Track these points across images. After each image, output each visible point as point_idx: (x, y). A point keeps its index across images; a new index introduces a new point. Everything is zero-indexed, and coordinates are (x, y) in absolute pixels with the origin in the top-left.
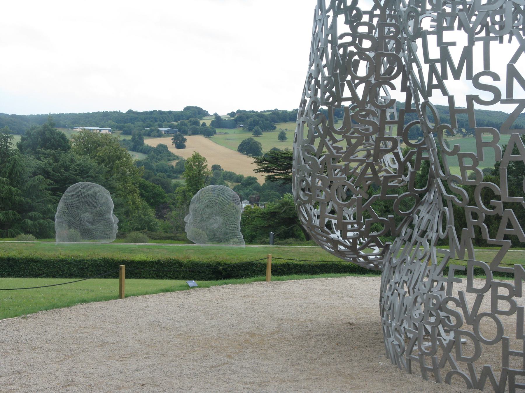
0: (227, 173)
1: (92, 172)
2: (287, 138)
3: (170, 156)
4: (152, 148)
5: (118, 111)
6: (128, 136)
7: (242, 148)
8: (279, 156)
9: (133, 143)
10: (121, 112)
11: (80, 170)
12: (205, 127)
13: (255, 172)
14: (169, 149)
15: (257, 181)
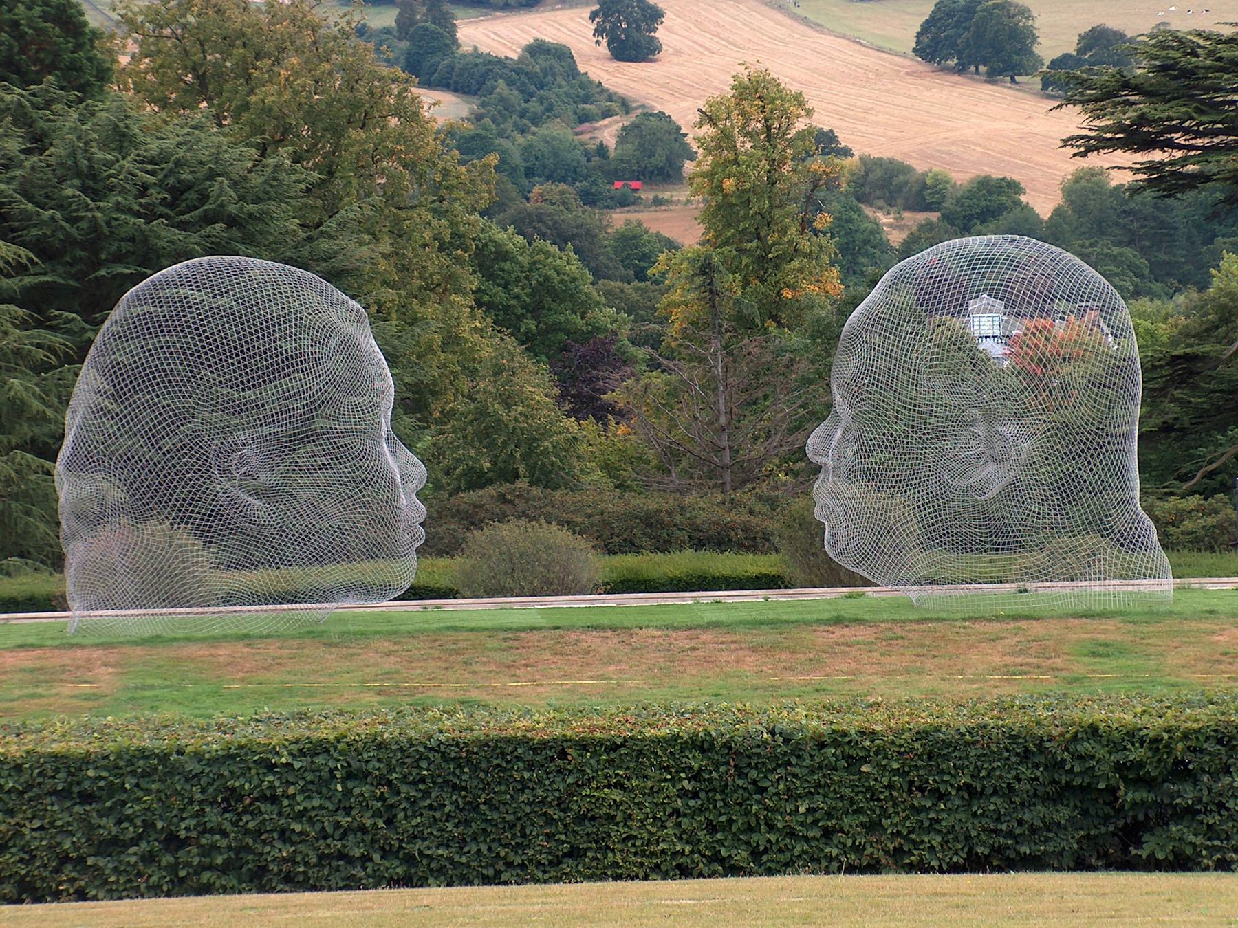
0: (869, 164)
1: (223, 193)
3: (587, 99)
4: (501, 62)
6: (382, 9)
7: (935, 41)
8: (1203, 61)
9: (405, 45)
11: (161, 184)
13: (1076, 150)
14: (582, 68)
15: (1023, 199)
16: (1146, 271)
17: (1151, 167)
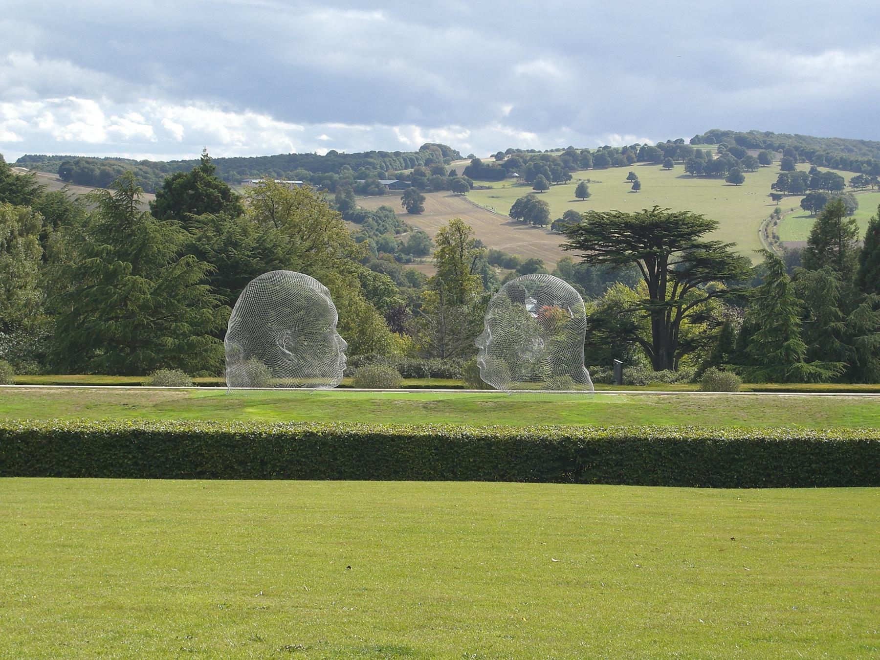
2: (590, 195)
5: (313, 153)
10: (318, 154)
12: (455, 177)
16: (584, 292)
17: (588, 256)
